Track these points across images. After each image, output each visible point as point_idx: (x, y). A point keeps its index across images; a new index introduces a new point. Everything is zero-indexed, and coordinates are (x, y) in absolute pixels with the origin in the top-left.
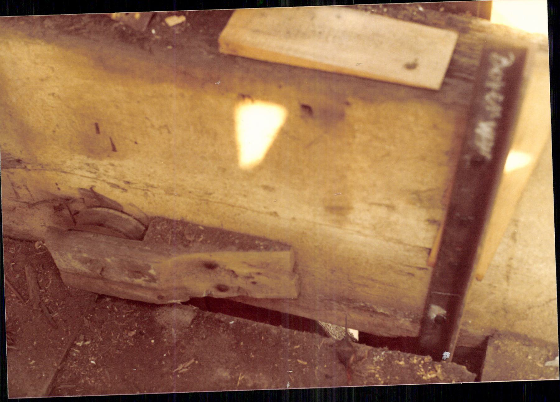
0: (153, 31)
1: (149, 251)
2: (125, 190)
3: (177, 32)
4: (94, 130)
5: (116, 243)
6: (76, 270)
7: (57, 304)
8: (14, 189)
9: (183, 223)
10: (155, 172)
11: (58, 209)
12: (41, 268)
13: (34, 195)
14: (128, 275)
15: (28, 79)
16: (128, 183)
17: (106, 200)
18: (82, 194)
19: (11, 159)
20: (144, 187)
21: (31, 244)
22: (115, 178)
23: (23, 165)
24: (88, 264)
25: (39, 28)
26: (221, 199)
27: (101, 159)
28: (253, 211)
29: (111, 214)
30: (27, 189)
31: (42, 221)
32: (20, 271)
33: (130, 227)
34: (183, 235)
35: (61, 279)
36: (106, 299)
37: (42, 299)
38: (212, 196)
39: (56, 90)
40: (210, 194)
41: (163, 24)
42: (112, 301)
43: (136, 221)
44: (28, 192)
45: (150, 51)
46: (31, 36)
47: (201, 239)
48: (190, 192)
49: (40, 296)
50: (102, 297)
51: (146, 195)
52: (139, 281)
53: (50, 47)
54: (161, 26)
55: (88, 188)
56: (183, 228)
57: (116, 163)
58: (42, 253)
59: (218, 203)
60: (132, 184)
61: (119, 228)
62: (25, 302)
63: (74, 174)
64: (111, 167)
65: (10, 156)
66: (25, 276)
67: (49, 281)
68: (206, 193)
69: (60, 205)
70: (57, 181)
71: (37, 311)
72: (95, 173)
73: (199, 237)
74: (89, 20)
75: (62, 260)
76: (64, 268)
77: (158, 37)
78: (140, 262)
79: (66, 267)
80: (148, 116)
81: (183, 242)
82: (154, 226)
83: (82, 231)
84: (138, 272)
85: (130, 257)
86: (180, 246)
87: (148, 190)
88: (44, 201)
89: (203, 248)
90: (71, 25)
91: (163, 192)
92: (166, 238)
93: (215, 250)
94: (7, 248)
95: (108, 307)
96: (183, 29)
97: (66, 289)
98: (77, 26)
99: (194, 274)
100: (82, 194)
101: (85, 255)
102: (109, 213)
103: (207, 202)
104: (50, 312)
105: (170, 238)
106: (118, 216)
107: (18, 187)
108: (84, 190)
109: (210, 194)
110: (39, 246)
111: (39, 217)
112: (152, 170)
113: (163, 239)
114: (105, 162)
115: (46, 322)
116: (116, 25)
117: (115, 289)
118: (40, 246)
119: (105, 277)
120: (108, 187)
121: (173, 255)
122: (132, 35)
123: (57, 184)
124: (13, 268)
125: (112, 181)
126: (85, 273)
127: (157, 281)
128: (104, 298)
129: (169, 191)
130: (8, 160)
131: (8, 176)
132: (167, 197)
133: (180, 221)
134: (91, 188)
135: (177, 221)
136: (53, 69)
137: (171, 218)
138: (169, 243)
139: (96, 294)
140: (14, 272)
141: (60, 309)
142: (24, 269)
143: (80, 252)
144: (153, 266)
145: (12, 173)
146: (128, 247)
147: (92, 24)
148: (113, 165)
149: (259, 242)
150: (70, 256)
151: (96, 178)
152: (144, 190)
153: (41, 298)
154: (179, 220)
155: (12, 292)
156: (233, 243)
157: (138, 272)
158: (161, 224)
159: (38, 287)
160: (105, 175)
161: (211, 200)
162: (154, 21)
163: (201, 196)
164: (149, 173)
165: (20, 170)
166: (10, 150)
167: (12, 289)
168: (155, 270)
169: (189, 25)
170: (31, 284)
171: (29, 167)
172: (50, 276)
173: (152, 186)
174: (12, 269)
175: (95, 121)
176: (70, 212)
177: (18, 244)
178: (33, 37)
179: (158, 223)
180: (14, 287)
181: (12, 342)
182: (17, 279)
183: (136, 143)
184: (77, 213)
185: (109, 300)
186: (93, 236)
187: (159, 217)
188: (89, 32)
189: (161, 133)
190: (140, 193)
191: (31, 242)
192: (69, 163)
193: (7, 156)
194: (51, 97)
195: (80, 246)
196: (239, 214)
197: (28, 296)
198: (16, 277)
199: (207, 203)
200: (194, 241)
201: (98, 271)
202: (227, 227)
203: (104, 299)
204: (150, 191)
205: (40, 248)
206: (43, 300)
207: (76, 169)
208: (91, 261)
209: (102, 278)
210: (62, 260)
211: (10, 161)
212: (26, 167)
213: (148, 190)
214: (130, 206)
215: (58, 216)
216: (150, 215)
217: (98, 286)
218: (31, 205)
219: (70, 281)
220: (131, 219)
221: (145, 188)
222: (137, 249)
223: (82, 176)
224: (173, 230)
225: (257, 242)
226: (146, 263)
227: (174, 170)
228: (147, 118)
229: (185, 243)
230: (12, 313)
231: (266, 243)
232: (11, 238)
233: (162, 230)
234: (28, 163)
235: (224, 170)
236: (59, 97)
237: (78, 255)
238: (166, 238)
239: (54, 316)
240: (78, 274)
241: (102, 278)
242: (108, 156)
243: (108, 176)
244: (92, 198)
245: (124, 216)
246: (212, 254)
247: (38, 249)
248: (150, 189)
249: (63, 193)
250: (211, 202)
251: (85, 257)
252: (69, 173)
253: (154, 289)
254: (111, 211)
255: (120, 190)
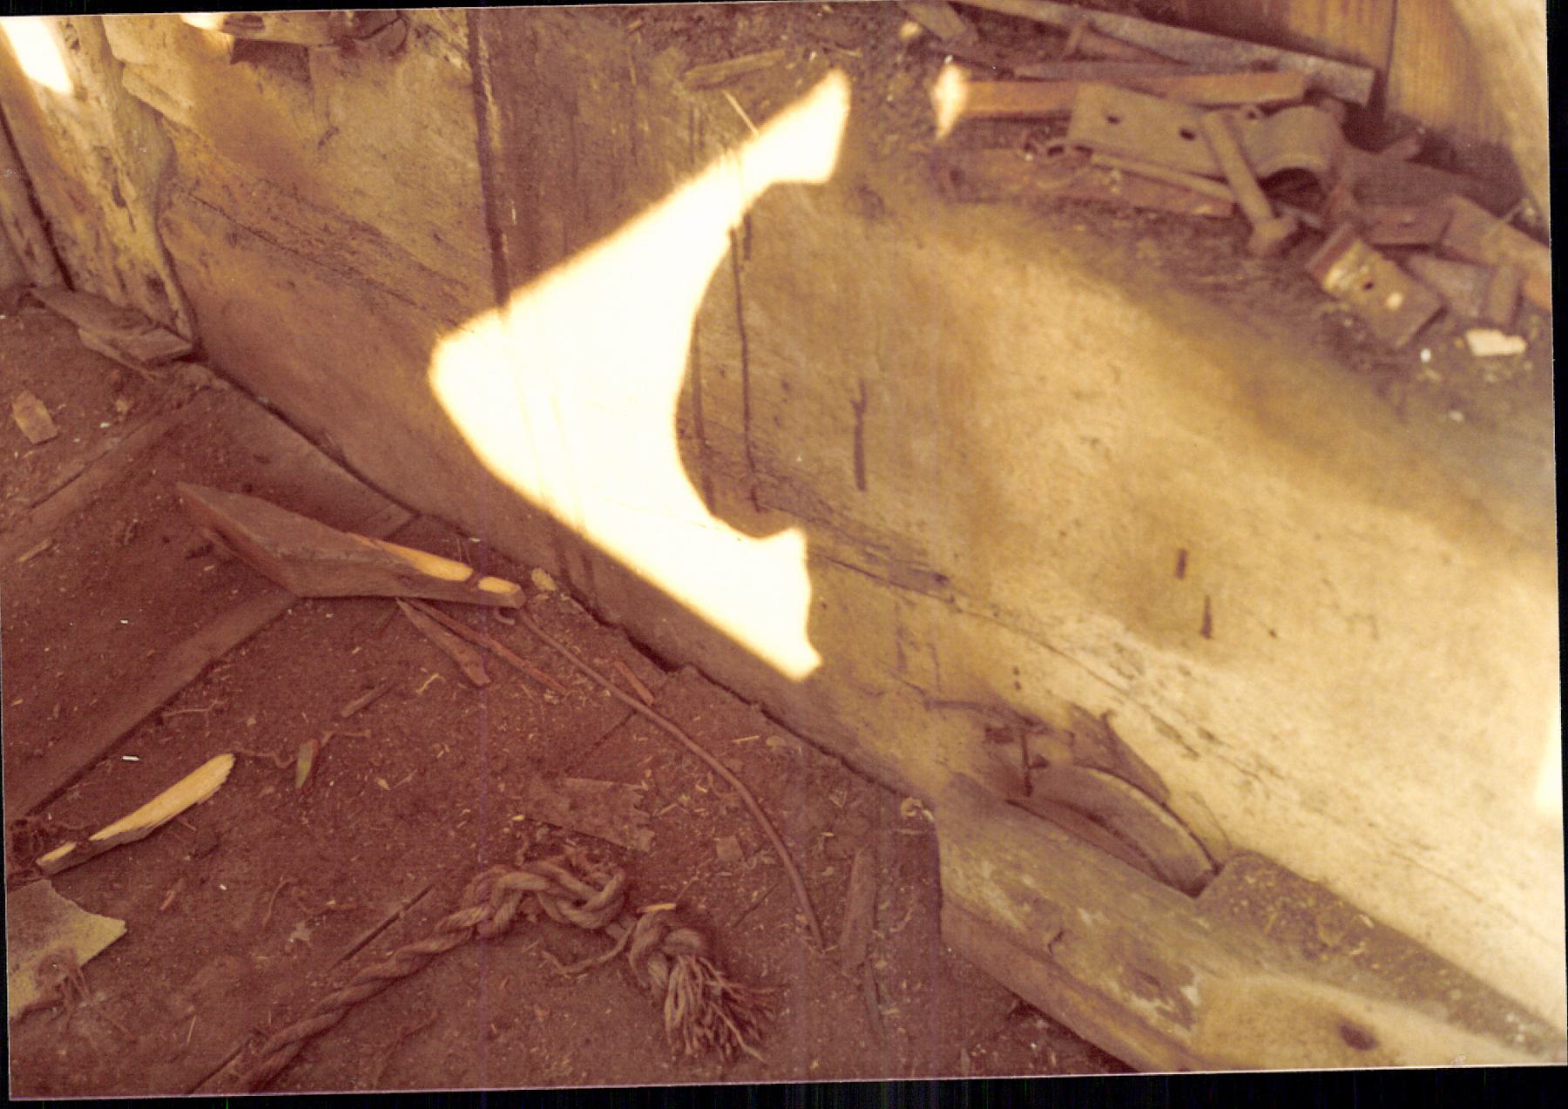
0: (1426, 355)
1: (1206, 934)
2: (1192, 753)
3: (1490, 378)
4: (1172, 565)
5: (1122, 878)
6: (987, 912)
7: (904, 985)
8: (898, 644)
9: (1323, 892)
10: (1295, 732)
11: (995, 736)
12: (896, 872)
13: (944, 677)
14: (1120, 979)
15: (1042, 379)
16: (1210, 737)
17: (1134, 763)
18: (1077, 724)
19: (923, 568)
20: (1249, 764)
21: (892, 796)
22: (1180, 712)
23: (947, 594)
24: (1027, 908)
25: (1118, 254)
26: (1451, 871)
27: (1159, 646)
28: (1531, 932)
29: (1136, 801)
30: (934, 656)
31: (941, 750)
32: (842, 860)
33: (1170, 851)
34: (1312, 923)
35: (939, 920)
36: (1035, 1021)
37: (870, 956)
38: (1427, 854)
39: (1106, 435)
40: (1426, 848)
41: (1459, 343)
42: (1049, 1032)
43: (1194, 843)
44: (933, 665)
45: (1400, 412)
46: (1093, 269)
47: (1356, 952)
48: (1371, 825)
49: (868, 946)
50: (1026, 1010)
51: (1246, 787)
52: (1146, 1007)
53: (1133, 313)
54: (1451, 346)
55: (1097, 713)
56: (1317, 906)
57: (1199, 669)
58: (912, 833)
59: (1439, 876)
60: (1220, 743)
61: (1143, 844)
62: (824, 946)
63: (1072, 661)
64: (1180, 678)
65: (921, 559)
66: (849, 879)
67: (905, 915)
68: (1416, 843)
69: (1007, 728)
70: (1019, 665)
71: (848, 984)
72: (1131, 677)
73: (1354, 945)
74: (1259, 273)
75: (960, 872)
76: (958, 895)
77: (1433, 375)
78: (1168, 954)
79: (964, 894)
80: (1330, 578)
81: (1304, 942)
82: (1240, 872)
83: (1042, 817)
84: (1153, 980)
85: (1146, 928)
86: (1294, 951)
87: (1256, 777)
88: (973, 706)
89: (1355, 978)
90: (1211, 272)
91: (1296, 797)
92: (1261, 913)
93: (1385, 997)
94: (829, 787)
95: (1033, 1045)
96: (1508, 374)
97: (942, 953)
98: (1223, 279)
99: (1304, 1043)
100: (1077, 724)
101: (1028, 881)
102: (1128, 797)
103: (1410, 863)
104: (879, 999)
105: (1273, 917)
106: (1149, 814)
107: (912, 643)
108: (1085, 712)
109: (1426, 848)
110: (909, 811)
111: (938, 739)
112: (1288, 726)
113: (1254, 914)
114: (1171, 657)
115: (861, 1020)
116: (1329, 307)
117: (1071, 1002)
118: (913, 814)
119: (1058, 960)
120: (1150, 728)
121: (1266, 965)
122: (1363, 347)
123: (1016, 672)
124: (825, 846)
125: (1169, 718)
126: (1009, 928)
127: (1195, 1027)
128: (1032, 1015)
129: (1315, 801)
130: (914, 567)
131: (897, 608)
132: (1302, 815)
133: (1314, 883)
134: (1105, 716)
135: (1306, 881)
136: (1117, 374)
137: (1293, 867)
138: (1268, 928)
139: (1015, 995)
140: (822, 856)
141: (909, 1000)
142: (851, 857)
143: (1018, 867)
144: (1199, 977)
145: (911, 604)
146: (1153, 900)
147: (1265, 285)
148: (1187, 673)
149: (1518, 1020)
150: (987, 869)
151: (1126, 693)
152: (1244, 772)
153: (868, 953)
154: (1314, 880)
155: (799, 910)
156: (1443, 997)
157: (1152, 979)
158: (1259, 873)
159: (871, 922)
160: (1154, 693)
161: (1421, 862)
162: (1436, 327)
163: (1398, 846)
164: (1275, 731)
165: (936, 603)
166: (928, 542)
167: (804, 900)
168: (1201, 992)
169: (1528, 366)
170: (857, 906)
171: (962, 602)
172: (911, 902)
173: (1272, 771)
174: (821, 847)
175: (1179, 545)
176: (1026, 757)
177: (860, 785)
178: (1099, 272)
179: (1255, 869)
180: (809, 897)
181: (757, 1037)
182: (824, 877)
183: (1273, 634)
184: (1042, 764)
185: (1044, 1029)
186: (1068, 842)
187: (1260, 855)
188: (1250, 304)
189: (1351, 631)
190: (1231, 774)
191: (894, 792)
192: (1071, 626)
193: (916, 558)
194: (1086, 448)
195: (1024, 853)
196: (1487, 926)
197: (839, 933)
198: (824, 874)
199: (1408, 867)
200: (1336, 950)
201: (1048, 937)
202: (1440, 944)
203: (1030, 1020)
204: (1260, 781)
205: (910, 819)
206: (871, 960)
207: (1083, 648)
208: (1037, 903)
209: (1048, 959)
210: (960, 872)
211: (917, 572)
212: (952, 600)
213: (1256, 777)
214: (1191, 801)
215: (989, 753)
216: (1235, 839)
217: (1030, 979)
218: (937, 704)
219: (959, 933)
220: (1182, 832)
221: (1251, 769)
222: (1172, 914)
223: (1091, 673)
224: (1288, 900)
225: (1510, 1018)
226: (1185, 962)
227: (1349, 746)
228: (1326, 582)
229: (1310, 946)
230: (782, 963)
231: (1536, 1030)
232: (844, 762)
233: (1257, 890)
234: (962, 593)
235: (1490, 796)
236: (1107, 455)
237: (1010, 874)
238: (1261, 913)
239: (887, 1012)
240: (985, 922)
241: (1048, 959)
242: (1184, 644)
243: (1162, 700)
244: (1097, 742)
245: (1166, 819)
246: (1375, 1005)
247: (905, 818)
248: (1263, 774)
249: (1026, 702)
250: (1420, 867)
251: (1027, 888)
252: (1061, 654)
253: (1178, 1046)
254: (1136, 795)
255: (1180, 749)
